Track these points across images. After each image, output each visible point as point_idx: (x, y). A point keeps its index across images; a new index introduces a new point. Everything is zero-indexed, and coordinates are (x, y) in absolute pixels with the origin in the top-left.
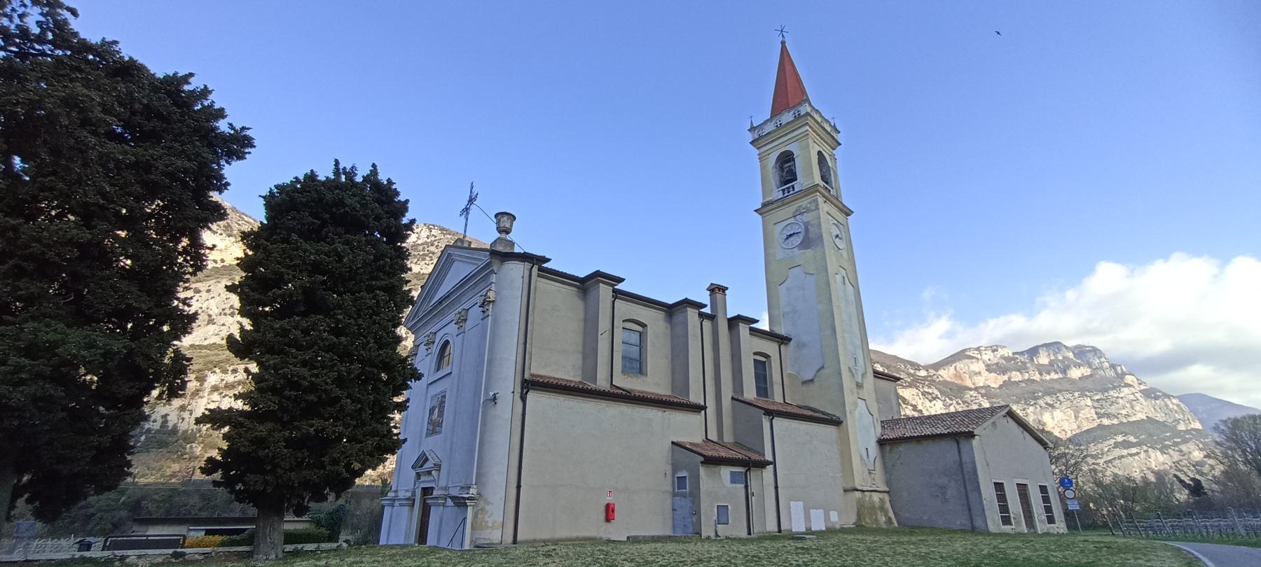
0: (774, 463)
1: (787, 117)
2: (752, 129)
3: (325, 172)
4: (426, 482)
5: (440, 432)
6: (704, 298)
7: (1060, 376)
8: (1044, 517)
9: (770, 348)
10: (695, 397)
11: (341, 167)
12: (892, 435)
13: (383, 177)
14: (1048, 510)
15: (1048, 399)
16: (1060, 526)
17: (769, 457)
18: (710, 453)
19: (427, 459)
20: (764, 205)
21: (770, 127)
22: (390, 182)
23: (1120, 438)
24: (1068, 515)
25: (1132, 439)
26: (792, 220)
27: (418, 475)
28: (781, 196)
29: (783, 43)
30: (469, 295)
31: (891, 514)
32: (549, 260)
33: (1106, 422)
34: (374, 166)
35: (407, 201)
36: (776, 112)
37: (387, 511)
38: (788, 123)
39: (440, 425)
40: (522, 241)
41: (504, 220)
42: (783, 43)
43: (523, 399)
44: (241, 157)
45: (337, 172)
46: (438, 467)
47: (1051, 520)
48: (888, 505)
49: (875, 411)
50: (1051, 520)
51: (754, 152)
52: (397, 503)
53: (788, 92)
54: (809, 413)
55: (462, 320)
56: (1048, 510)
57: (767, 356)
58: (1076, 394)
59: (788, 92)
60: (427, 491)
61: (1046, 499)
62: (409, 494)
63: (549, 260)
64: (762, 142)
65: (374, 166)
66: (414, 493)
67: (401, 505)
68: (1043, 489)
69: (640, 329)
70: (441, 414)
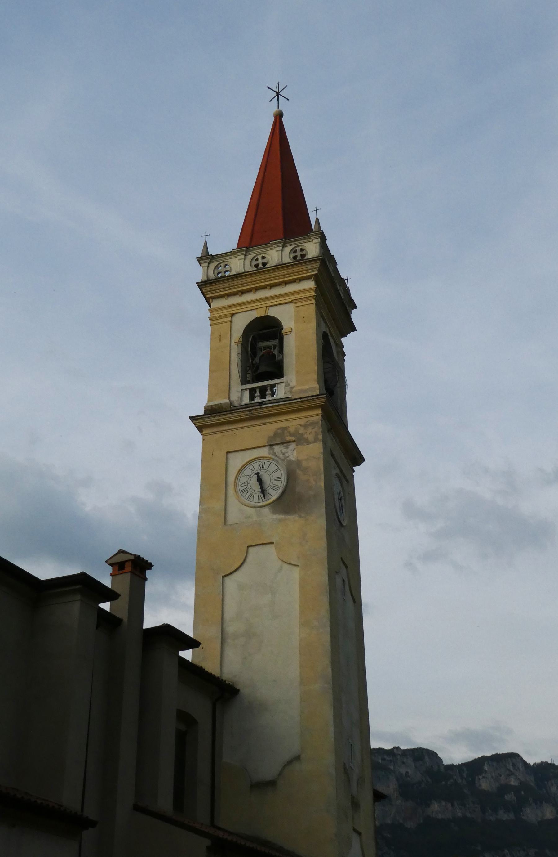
1: (275, 255)
2: (206, 258)
7: (511, 816)
9: (199, 707)
10: (69, 798)
20: (210, 411)
21: (237, 265)
26: (264, 452)
29: (279, 116)
36: (254, 235)
38: (281, 266)
42: (279, 116)
53: (280, 204)
59: (280, 204)
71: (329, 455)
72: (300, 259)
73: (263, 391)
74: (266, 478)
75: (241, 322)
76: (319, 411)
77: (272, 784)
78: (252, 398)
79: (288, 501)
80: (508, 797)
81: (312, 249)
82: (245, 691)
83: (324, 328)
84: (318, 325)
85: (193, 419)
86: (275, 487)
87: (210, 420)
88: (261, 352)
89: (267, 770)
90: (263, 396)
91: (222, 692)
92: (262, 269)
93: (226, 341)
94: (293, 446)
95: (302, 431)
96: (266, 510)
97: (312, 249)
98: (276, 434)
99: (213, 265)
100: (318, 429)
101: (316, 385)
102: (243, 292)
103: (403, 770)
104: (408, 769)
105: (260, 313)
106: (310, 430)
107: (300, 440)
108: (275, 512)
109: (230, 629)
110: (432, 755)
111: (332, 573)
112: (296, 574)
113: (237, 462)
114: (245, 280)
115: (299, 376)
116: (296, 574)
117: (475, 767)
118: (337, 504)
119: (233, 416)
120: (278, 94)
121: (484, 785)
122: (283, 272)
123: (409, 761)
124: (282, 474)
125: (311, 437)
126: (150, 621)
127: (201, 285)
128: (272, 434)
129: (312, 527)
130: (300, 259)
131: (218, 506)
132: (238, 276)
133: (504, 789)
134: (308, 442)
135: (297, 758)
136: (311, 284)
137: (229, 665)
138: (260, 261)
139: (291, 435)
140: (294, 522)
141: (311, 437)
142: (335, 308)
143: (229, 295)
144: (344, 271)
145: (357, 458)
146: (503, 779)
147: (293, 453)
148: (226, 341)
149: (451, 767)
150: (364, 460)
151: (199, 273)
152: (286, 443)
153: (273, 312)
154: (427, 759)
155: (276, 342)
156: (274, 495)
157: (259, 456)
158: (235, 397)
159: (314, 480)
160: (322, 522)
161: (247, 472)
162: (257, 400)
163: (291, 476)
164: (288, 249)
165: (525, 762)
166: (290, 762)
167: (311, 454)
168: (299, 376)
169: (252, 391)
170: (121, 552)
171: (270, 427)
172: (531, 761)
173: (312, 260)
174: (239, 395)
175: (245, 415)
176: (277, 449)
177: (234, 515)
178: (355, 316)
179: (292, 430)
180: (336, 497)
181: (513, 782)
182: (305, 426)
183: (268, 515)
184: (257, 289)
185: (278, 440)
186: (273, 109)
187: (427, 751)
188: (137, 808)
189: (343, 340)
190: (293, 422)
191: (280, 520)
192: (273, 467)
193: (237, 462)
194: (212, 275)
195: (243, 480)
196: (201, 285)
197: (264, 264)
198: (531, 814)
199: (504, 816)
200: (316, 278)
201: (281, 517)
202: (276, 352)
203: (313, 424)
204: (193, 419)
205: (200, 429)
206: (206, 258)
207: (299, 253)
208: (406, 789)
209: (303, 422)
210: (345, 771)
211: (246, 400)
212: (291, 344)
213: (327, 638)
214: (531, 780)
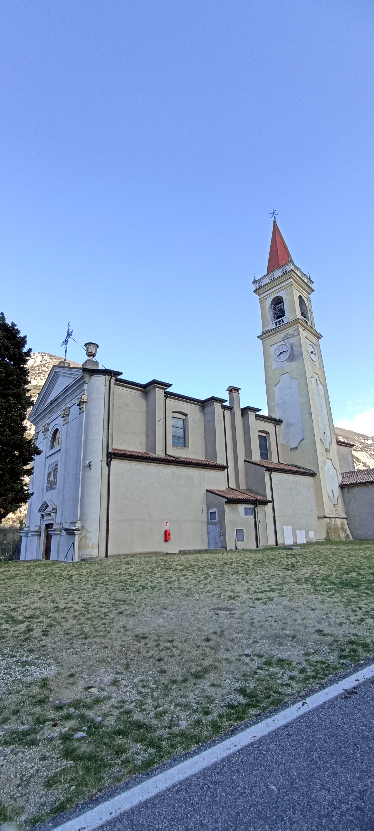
0: (272, 501)
2: (255, 282)
4: (48, 520)
5: (55, 488)
6: (225, 396)
9: (269, 427)
10: (221, 461)
17: (269, 498)
18: (231, 497)
20: (264, 333)
21: (267, 281)
22: (13, 324)
26: (282, 343)
27: (43, 516)
32: (121, 374)
36: (271, 269)
38: (279, 277)
39: (55, 483)
41: (91, 348)
43: (108, 465)
46: (55, 510)
48: (346, 527)
49: (337, 465)
59: (279, 256)
62: (37, 529)
63: (121, 374)
64: (262, 290)
67: (32, 536)
70: (55, 477)
78: (277, 325)
85: (258, 337)
87: (264, 336)
92: (273, 280)
98: (285, 336)
106: (296, 332)
114: (268, 286)
119: (270, 333)
122: (298, 279)
127: (255, 291)
128: (284, 336)
134: (296, 336)
138: (272, 278)
139: (290, 335)
151: (253, 287)
153: (278, 294)
157: (93, 342)
162: (278, 326)
169: (276, 323)
171: (282, 335)
175: (274, 332)
179: (290, 333)
182: (294, 331)
184: (273, 288)
191: (290, 364)
194: (258, 287)
196: (255, 291)
197: (274, 278)
201: (290, 363)
202: (282, 308)
204: (258, 337)
205: (261, 339)
206: (255, 282)
207: (284, 271)
209: (293, 329)
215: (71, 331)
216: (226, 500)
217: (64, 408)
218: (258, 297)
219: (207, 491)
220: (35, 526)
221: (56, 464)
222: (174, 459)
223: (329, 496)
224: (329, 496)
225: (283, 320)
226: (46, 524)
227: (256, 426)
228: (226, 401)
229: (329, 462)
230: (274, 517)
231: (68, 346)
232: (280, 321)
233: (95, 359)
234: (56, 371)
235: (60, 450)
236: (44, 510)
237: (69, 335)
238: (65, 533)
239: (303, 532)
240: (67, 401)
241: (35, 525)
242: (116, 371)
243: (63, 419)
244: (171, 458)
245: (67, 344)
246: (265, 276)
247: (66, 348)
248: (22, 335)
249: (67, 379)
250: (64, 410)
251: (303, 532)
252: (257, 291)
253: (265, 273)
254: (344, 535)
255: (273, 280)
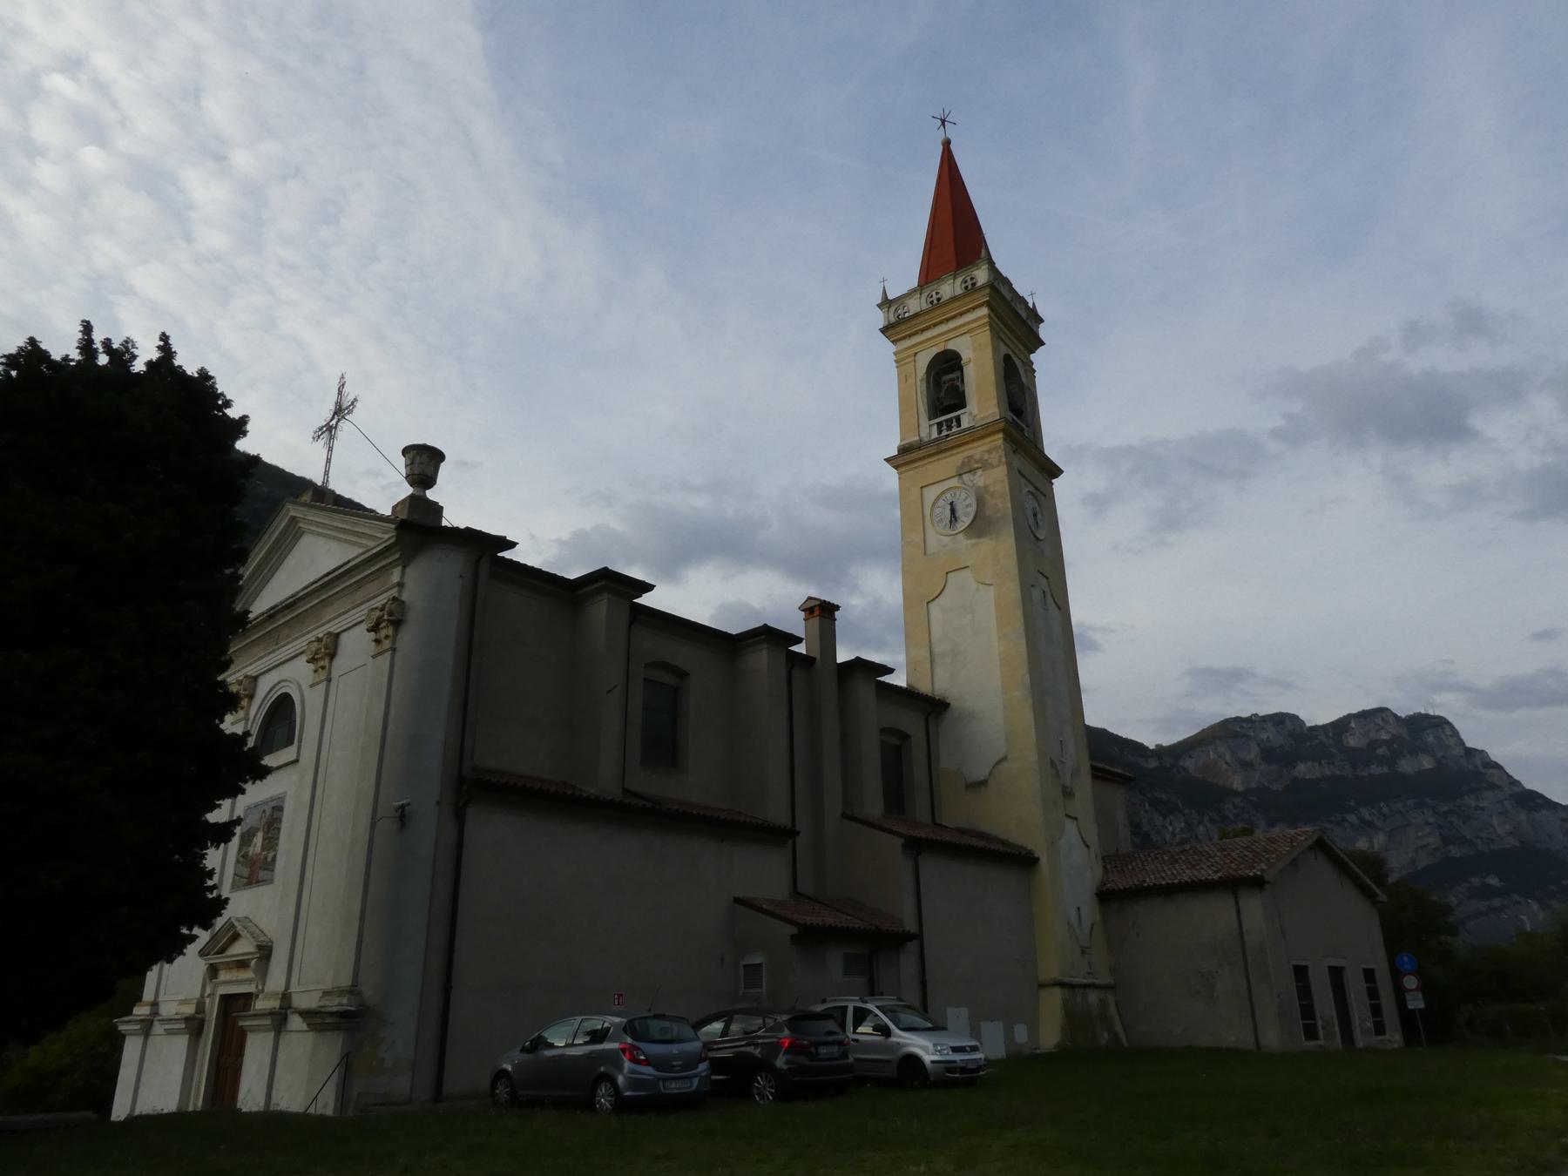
0: (918, 937)
1: (949, 288)
2: (886, 303)
3: (62, 345)
4: (234, 983)
5: (269, 881)
6: (794, 623)
7: (1386, 770)
8: (1369, 1024)
9: (911, 723)
10: (776, 813)
11: (98, 337)
12: (1123, 884)
13: (188, 361)
14: (1376, 1010)
15: (1365, 812)
16: (1394, 1037)
17: (910, 926)
18: (809, 919)
19: (236, 937)
20: (903, 450)
21: (914, 306)
22: (204, 376)
23: (1476, 881)
24: (1407, 1019)
25: (1494, 881)
26: (954, 482)
27: (213, 971)
28: (935, 435)
29: (947, 144)
30: (340, 606)
31: (1119, 1028)
32: (512, 545)
33: (1454, 851)
34: (164, 337)
35: (244, 420)
36: (931, 272)
37: (131, 1048)
38: (954, 299)
39: (269, 866)
40: (461, 505)
41: (424, 462)
42: (947, 144)
43: (460, 816)
44: (244, 433)
45: (87, 346)
46: (265, 952)
47: (1380, 1029)
48: (1113, 1010)
49: (1093, 839)
50: (1380, 1029)
51: (887, 347)
52: (158, 1028)
53: (956, 234)
54: (982, 844)
55: (327, 651)
56: (1376, 1010)
57: (683, 675)
58: (1410, 802)
59: (956, 234)
60: (234, 1005)
61: (1373, 993)
62: (190, 1010)
63: (512, 545)
64: (904, 330)
65: (164, 337)
66: (200, 1007)
67: (170, 1032)
68: (1369, 975)
69: (670, 679)
70: (271, 841)
71: (1016, 475)
72: (972, 289)
73: (949, 424)
74: (960, 509)
75: (924, 360)
76: (1001, 435)
77: (984, 783)
78: (940, 431)
79: (980, 526)
80: (1380, 751)
81: (981, 275)
82: (954, 704)
83: (1004, 350)
84: (995, 349)
85: (887, 460)
86: (966, 514)
87: (906, 457)
88: (943, 385)
89: (979, 772)
90: (949, 428)
91: (932, 708)
92: (937, 305)
93: (911, 381)
94: (980, 472)
95: (986, 456)
96: (960, 537)
97: (981, 275)
99: (892, 310)
100: (1001, 453)
101: (996, 410)
102: (922, 331)
103: (1264, 736)
104: (1270, 734)
105: (941, 348)
107: (985, 466)
108: (968, 537)
109: (937, 650)
110: (1294, 718)
111: (1026, 588)
112: (991, 593)
113: (931, 494)
115: (982, 401)
116: (991, 593)
117: (1342, 725)
118: (1031, 520)
120: (943, 122)
121: (1353, 742)
123: (1269, 726)
124: (972, 500)
125: (994, 461)
126: (843, 656)
127: (884, 330)
129: (1001, 548)
130: (972, 289)
131: (918, 538)
132: (916, 315)
133: (1375, 744)
135: (1005, 759)
136: (984, 311)
137: (940, 684)
140: (986, 544)
141: (994, 461)
142: (1017, 326)
143: (910, 336)
144: (1021, 288)
145: (1054, 471)
146: (1373, 735)
147: (980, 479)
148: (911, 381)
149: (1315, 728)
150: (1061, 472)
151: (880, 319)
152: (972, 471)
153: (951, 346)
154: (1288, 723)
155: (958, 373)
156: (965, 521)
158: (924, 434)
159: (1002, 503)
160: (1012, 540)
161: (941, 503)
163: (980, 501)
164: (959, 280)
165: (1395, 716)
166: (998, 763)
167: (996, 478)
168: (982, 401)
169: (940, 425)
170: (810, 598)
171: (957, 458)
172: (1403, 714)
173: (983, 287)
174: (928, 430)
176: (965, 477)
177: (933, 546)
178: (1043, 332)
179: (977, 457)
180: (1030, 514)
181: (1384, 736)
182: (989, 452)
183: (964, 542)
185: (965, 469)
186: (940, 136)
187: (1288, 715)
188: (844, 816)
189: (1033, 357)
190: (978, 450)
192: (964, 495)
193: (931, 494)
194: (893, 320)
195: (937, 511)
196: (884, 330)
198: (1405, 766)
199: (1376, 770)
200: (988, 304)
203: (996, 448)
204: (887, 460)
205: (896, 467)
208: (1268, 754)
209: (986, 448)
210: (1052, 766)
211: (935, 435)
212: (970, 373)
213: (1023, 648)
214: (1405, 733)
215: (351, 398)
216: (793, 930)
217: (320, 633)
218: (893, 348)
219: (737, 901)
220: (184, 1002)
221: (274, 804)
222: (649, 805)
223: (1069, 924)
224: (1069, 924)
225: (958, 419)
226: (222, 996)
227: (871, 715)
228: (798, 640)
229: (1070, 827)
230: (447, 990)
231: (337, 444)
232: (950, 421)
233: (431, 494)
234: (293, 518)
235: (297, 761)
236: (222, 951)
237: (340, 411)
238: (304, 1027)
239: (1000, 1025)
240: (329, 612)
241: (181, 997)
242: (1179, 743)
243: (312, 667)
244: (641, 803)
245: (332, 438)
246: (914, 291)
247: (330, 449)
248: (233, 413)
249: (333, 545)
250: (319, 640)
251: (1000, 1025)
252: (891, 332)
253: (914, 282)
254: (1106, 1036)
255: (937, 305)
